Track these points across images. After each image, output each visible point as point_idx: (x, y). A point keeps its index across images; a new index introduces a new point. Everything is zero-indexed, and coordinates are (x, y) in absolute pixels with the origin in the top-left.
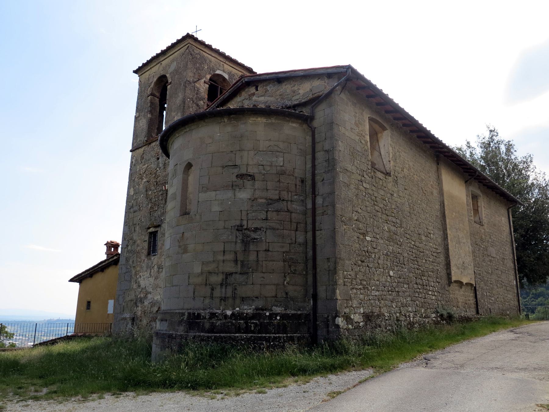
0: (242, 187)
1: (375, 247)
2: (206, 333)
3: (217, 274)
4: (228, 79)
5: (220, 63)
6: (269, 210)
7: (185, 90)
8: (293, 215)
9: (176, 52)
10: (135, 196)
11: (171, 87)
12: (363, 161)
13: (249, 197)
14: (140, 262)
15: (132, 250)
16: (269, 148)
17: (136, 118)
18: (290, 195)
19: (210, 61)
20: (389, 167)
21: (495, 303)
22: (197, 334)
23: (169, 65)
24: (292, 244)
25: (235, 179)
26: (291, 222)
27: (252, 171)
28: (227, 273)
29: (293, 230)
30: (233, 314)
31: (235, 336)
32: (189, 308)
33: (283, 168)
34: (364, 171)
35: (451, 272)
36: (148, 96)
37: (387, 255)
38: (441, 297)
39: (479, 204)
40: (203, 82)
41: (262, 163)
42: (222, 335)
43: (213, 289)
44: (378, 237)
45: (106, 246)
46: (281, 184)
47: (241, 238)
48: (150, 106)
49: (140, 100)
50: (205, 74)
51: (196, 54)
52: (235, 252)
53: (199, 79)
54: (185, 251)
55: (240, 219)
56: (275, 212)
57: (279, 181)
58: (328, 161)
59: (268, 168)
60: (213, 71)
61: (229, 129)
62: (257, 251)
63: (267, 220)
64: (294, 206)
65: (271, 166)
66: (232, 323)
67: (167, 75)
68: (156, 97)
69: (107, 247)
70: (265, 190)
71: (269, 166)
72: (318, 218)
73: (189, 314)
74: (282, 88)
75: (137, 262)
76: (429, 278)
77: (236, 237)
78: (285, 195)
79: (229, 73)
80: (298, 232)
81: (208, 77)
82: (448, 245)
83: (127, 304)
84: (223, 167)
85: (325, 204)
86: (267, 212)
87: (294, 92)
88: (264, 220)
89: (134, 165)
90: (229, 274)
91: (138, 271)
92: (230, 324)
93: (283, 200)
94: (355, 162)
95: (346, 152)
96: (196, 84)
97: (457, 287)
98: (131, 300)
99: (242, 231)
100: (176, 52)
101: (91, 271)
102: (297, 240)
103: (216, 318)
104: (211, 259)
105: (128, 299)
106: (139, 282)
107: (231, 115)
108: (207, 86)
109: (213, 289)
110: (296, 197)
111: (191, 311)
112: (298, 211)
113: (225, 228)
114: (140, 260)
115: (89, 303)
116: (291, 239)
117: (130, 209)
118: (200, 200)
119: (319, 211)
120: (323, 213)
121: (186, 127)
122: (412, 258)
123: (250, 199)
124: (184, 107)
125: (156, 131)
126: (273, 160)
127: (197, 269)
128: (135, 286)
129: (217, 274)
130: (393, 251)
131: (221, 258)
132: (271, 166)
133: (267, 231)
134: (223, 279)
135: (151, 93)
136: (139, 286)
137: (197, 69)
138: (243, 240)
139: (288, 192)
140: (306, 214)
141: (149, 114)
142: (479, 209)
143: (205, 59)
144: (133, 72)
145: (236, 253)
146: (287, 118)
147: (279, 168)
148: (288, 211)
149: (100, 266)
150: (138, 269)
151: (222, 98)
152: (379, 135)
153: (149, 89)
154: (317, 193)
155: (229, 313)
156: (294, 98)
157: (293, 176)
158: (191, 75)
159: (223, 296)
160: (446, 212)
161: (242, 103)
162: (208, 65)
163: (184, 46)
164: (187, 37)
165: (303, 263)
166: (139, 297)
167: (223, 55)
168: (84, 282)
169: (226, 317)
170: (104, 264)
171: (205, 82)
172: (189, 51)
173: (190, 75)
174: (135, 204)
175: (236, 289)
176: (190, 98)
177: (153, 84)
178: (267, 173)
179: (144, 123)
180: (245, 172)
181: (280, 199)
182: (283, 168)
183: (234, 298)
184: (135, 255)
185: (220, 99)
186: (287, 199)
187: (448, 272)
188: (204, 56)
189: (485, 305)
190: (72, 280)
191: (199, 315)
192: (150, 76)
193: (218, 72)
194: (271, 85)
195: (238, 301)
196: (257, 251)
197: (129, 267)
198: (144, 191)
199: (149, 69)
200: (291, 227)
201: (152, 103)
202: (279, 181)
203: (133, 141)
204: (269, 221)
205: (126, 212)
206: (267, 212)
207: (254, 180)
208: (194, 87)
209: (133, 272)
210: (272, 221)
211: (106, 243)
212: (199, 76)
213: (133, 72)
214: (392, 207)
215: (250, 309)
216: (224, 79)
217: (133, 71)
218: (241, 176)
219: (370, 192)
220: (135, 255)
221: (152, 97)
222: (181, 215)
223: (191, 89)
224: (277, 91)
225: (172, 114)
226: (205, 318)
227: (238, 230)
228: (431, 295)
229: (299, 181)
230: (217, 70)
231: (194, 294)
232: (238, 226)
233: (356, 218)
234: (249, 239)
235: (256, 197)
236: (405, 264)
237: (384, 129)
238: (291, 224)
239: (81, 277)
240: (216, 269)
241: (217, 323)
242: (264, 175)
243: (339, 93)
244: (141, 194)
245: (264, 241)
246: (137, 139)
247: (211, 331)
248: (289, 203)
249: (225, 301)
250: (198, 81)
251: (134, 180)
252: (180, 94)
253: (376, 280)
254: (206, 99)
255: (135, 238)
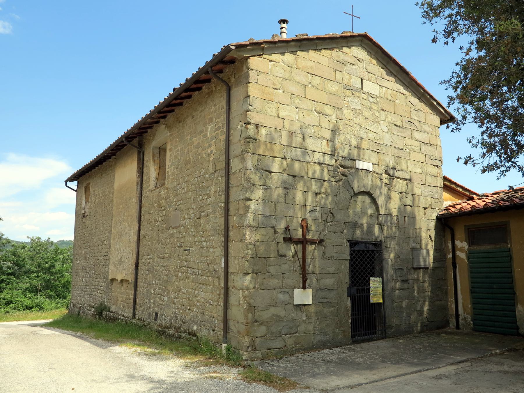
21: (168, 305)
38: (105, 295)
97: (119, 285)
189: (150, 307)
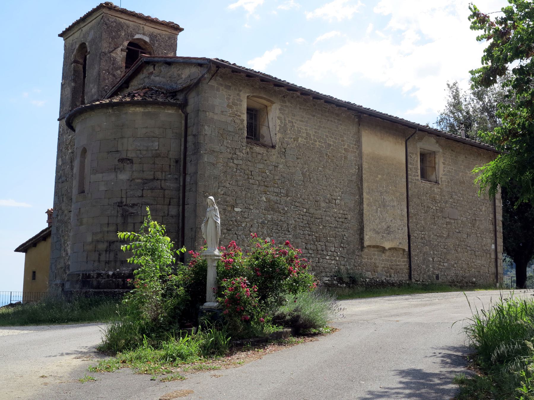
0: (122, 170)
1: (246, 217)
2: (94, 289)
3: (103, 242)
4: (149, 42)
5: (139, 26)
6: (144, 189)
7: (100, 61)
8: (167, 192)
9: (93, 20)
10: (62, 167)
11: (89, 57)
12: (236, 140)
13: (128, 178)
14: (67, 231)
15: (61, 220)
16: (146, 134)
17: (62, 85)
18: (164, 175)
19: (128, 27)
20: (275, 140)
22: (88, 290)
23: (87, 33)
24: (165, 216)
25: (117, 163)
26: (164, 198)
27: (131, 156)
28: (110, 241)
29: (166, 205)
30: (113, 274)
31: (115, 291)
32: (84, 270)
33: (158, 151)
34: (236, 149)
35: (363, 237)
36: (72, 64)
37: (263, 223)
39: (437, 161)
40: (120, 50)
41: (139, 148)
42: (105, 290)
43: (100, 255)
44: (252, 207)
45: (47, 214)
46: (156, 166)
47: (121, 213)
48: (74, 75)
49: (65, 66)
50: (122, 42)
51: (111, 23)
52: (116, 224)
53: (115, 49)
54: (81, 224)
55: (121, 197)
56: (149, 190)
57: (154, 163)
58: (194, 144)
59: (144, 152)
60: (131, 37)
61: (113, 119)
62: (134, 223)
63: (142, 197)
64: (167, 184)
65: (147, 150)
66: (112, 281)
67: (87, 44)
68: (79, 64)
69: (48, 215)
70: (141, 172)
71: (145, 150)
72: (187, 194)
73: (83, 274)
74: (171, 70)
75: (65, 232)
76: (327, 244)
77: (118, 212)
78: (159, 175)
79: (150, 35)
80: (170, 207)
81: (126, 44)
82: (363, 210)
83: (59, 272)
84: (108, 153)
85: (191, 183)
86: (143, 190)
87: (179, 75)
88: (140, 197)
89: (62, 135)
90: (112, 243)
91: (66, 241)
92: (111, 282)
93: (157, 179)
94: (224, 143)
95: (214, 135)
96: (112, 54)
98: (61, 268)
99: (122, 206)
100: (93, 20)
101: (34, 240)
102: (169, 213)
103: (101, 278)
104: (99, 231)
105: (59, 267)
106: (67, 250)
107: (114, 106)
108: (125, 54)
109: (100, 255)
110: (169, 176)
111: (84, 273)
112: (171, 188)
113: (109, 205)
114: (67, 229)
115: (34, 273)
116: (164, 213)
117: (59, 179)
118: (91, 181)
119: (187, 188)
120: (190, 189)
121: (82, 115)
122: (301, 224)
123: (129, 180)
124: (99, 80)
125: (81, 99)
126: (149, 145)
127: (89, 239)
128: (64, 254)
129: (103, 242)
130: (272, 219)
131: (106, 229)
132: (147, 150)
133: (142, 206)
134: (107, 247)
135: (74, 61)
136: (67, 254)
137: (113, 38)
138: (123, 214)
139: (162, 172)
140: (180, 190)
141: (73, 82)
142: (437, 166)
143: (121, 26)
144: (58, 36)
145: (117, 225)
146: (162, 107)
147: (154, 152)
148: (162, 188)
149: (42, 235)
150: (66, 238)
151: (127, 75)
152: (269, 108)
153: (72, 56)
154: (187, 172)
155: (111, 273)
156: (179, 82)
157: (168, 158)
158: (107, 46)
159: (107, 260)
160: (364, 176)
161: (144, 81)
162: (125, 32)
163: (99, 15)
164: (101, 7)
165: (175, 232)
166: (67, 264)
167: (140, 17)
168: (29, 251)
169: (108, 276)
170: (45, 233)
171: (122, 50)
172: (103, 21)
173: (105, 46)
174: (62, 175)
175: (117, 254)
176: (105, 70)
177: (75, 51)
178: (143, 157)
179: (68, 91)
180: (125, 157)
181: (154, 179)
182: (158, 151)
183: (116, 261)
184: (64, 224)
185: (126, 76)
186: (161, 178)
187: (362, 237)
188: (121, 22)
190: (17, 250)
191: (89, 274)
192: (73, 42)
193: (137, 36)
194: (164, 67)
195: (118, 264)
196: (134, 223)
197: (59, 236)
198: (69, 162)
199: (71, 35)
200: (164, 202)
201: (75, 71)
202: (154, 163)
203: (60, 109)
204: (145, 198)
205: (56, 183)
206: (143, 190)
207: (133, 163)
208: (110, 58)
209: (63, 241)
210: (146, 198)
211: (47, 211)
212: (115, 45)
213: (58, 36)
214: (275, 178)
215: (128, 270)
216: (145, 42)
217: (59, 35)
218: (122, 160)
219: (244, 167)
220: (64, 224)
221: (75, 64)
222: (79, 193)
223: (106, 60)
224: (168, 73)
225: (90, 85)
226: (94, 278)
227: (118, 206)
228: (329, 259)
229: (174, 161)
230: (135, 34)
231: (87, 259)
232: (119, 203)
233: (222, 192)
234: (127, 213)
235: (134, 178)
236: (290, 230)
237: (273, 103)
238: (164, 200)
239: (26, 247)
240: (103, 238)
241: (101, 281)
242: (141, 158)
243: (207, 80)
244: (67, 165)
245: (140, 215)
246: (63, 108)
247: (98, 287)
248: (163, 181)
249: (108, 263)
250: (114, 50)
251: (61, 150)
252: (96, 66)
253: (246, 245)
254: (124, 68)
255: (63, 208)
